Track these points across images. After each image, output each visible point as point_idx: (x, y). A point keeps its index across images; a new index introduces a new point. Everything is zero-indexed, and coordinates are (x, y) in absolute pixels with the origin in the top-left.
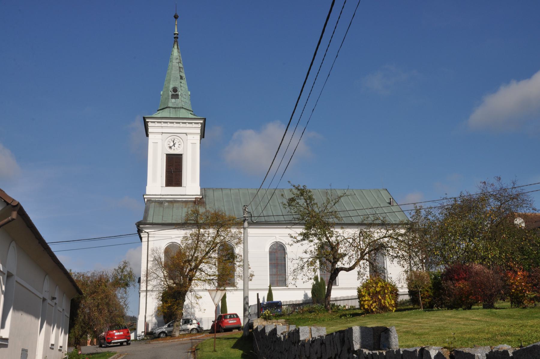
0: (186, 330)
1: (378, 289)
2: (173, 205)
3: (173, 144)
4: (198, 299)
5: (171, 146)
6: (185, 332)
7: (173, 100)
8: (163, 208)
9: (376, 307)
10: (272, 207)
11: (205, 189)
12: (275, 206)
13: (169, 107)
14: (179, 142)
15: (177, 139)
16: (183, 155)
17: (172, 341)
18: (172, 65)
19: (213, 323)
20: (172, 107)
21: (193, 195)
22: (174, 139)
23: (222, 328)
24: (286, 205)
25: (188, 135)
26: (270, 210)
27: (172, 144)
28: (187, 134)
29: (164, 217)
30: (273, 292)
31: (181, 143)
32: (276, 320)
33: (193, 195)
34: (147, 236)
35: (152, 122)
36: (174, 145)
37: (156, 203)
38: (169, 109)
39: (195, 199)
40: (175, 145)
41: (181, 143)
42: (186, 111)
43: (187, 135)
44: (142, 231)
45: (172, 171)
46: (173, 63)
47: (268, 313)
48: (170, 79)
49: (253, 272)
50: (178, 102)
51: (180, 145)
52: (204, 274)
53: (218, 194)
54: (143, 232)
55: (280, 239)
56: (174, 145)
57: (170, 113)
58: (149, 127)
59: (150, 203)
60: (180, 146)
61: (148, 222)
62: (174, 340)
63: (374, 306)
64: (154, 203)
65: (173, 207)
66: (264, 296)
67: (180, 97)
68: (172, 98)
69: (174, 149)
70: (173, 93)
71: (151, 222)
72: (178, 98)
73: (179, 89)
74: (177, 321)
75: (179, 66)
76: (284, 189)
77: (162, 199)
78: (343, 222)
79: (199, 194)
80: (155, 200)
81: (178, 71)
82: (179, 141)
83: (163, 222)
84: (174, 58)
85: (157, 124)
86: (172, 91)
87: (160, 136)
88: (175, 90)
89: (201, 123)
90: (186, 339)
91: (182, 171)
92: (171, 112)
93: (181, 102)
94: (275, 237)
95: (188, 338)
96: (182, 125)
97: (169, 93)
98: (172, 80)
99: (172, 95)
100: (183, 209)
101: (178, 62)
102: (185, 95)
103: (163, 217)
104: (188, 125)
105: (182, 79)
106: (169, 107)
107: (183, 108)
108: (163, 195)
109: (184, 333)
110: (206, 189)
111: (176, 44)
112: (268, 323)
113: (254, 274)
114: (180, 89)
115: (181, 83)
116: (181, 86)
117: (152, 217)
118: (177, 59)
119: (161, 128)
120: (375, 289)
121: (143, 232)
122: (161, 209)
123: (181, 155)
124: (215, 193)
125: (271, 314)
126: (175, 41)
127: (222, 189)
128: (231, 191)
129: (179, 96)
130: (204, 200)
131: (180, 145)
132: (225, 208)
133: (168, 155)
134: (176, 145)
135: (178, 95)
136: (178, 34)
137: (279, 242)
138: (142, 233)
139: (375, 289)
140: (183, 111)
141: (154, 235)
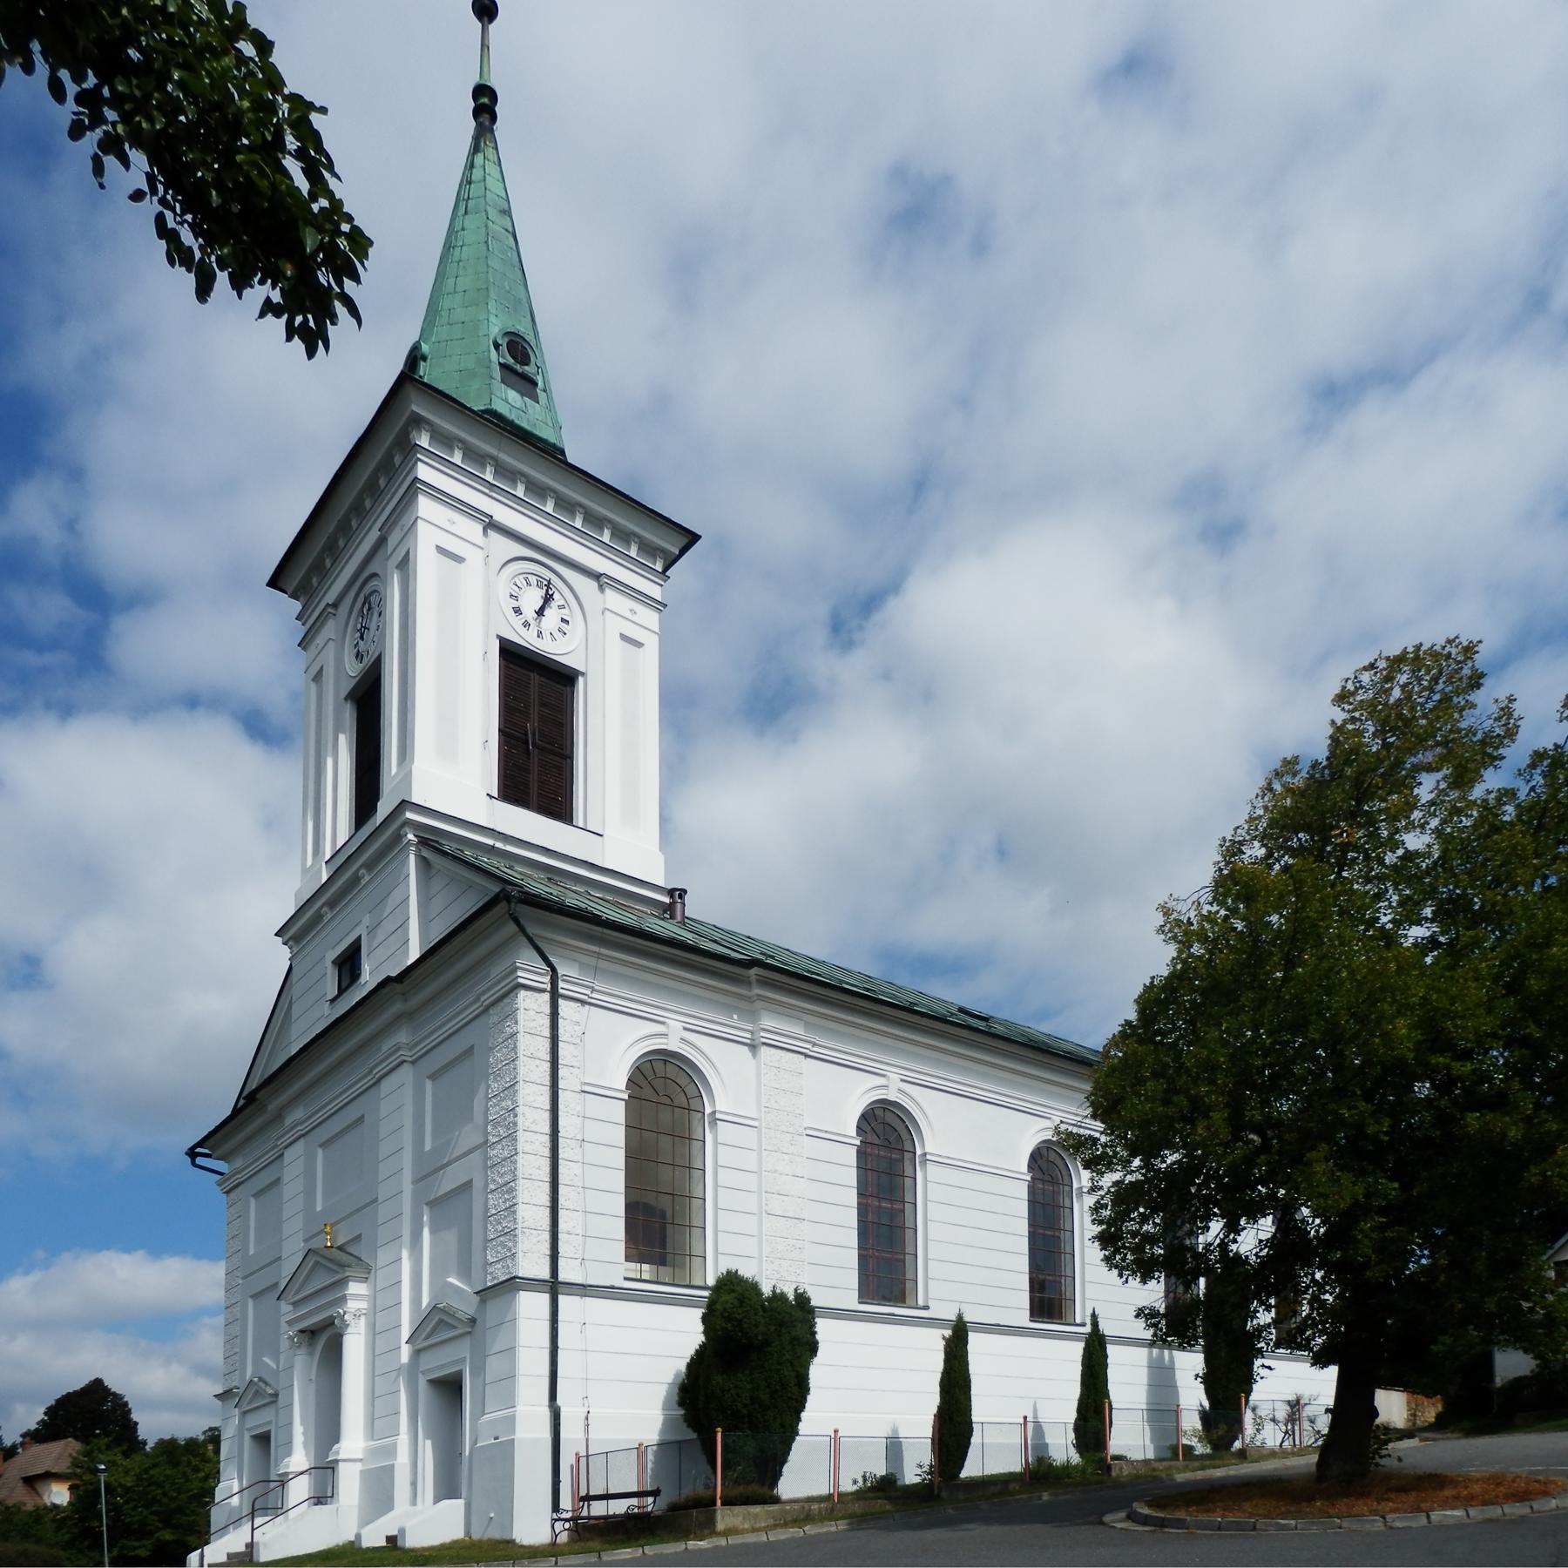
7: (513, 395)
16: (581, 679)
31: (572, 617)
35: (438, 436)
43: (601, 588)
70: (511, 361)
87: (474, 529)
98: (492, 295)
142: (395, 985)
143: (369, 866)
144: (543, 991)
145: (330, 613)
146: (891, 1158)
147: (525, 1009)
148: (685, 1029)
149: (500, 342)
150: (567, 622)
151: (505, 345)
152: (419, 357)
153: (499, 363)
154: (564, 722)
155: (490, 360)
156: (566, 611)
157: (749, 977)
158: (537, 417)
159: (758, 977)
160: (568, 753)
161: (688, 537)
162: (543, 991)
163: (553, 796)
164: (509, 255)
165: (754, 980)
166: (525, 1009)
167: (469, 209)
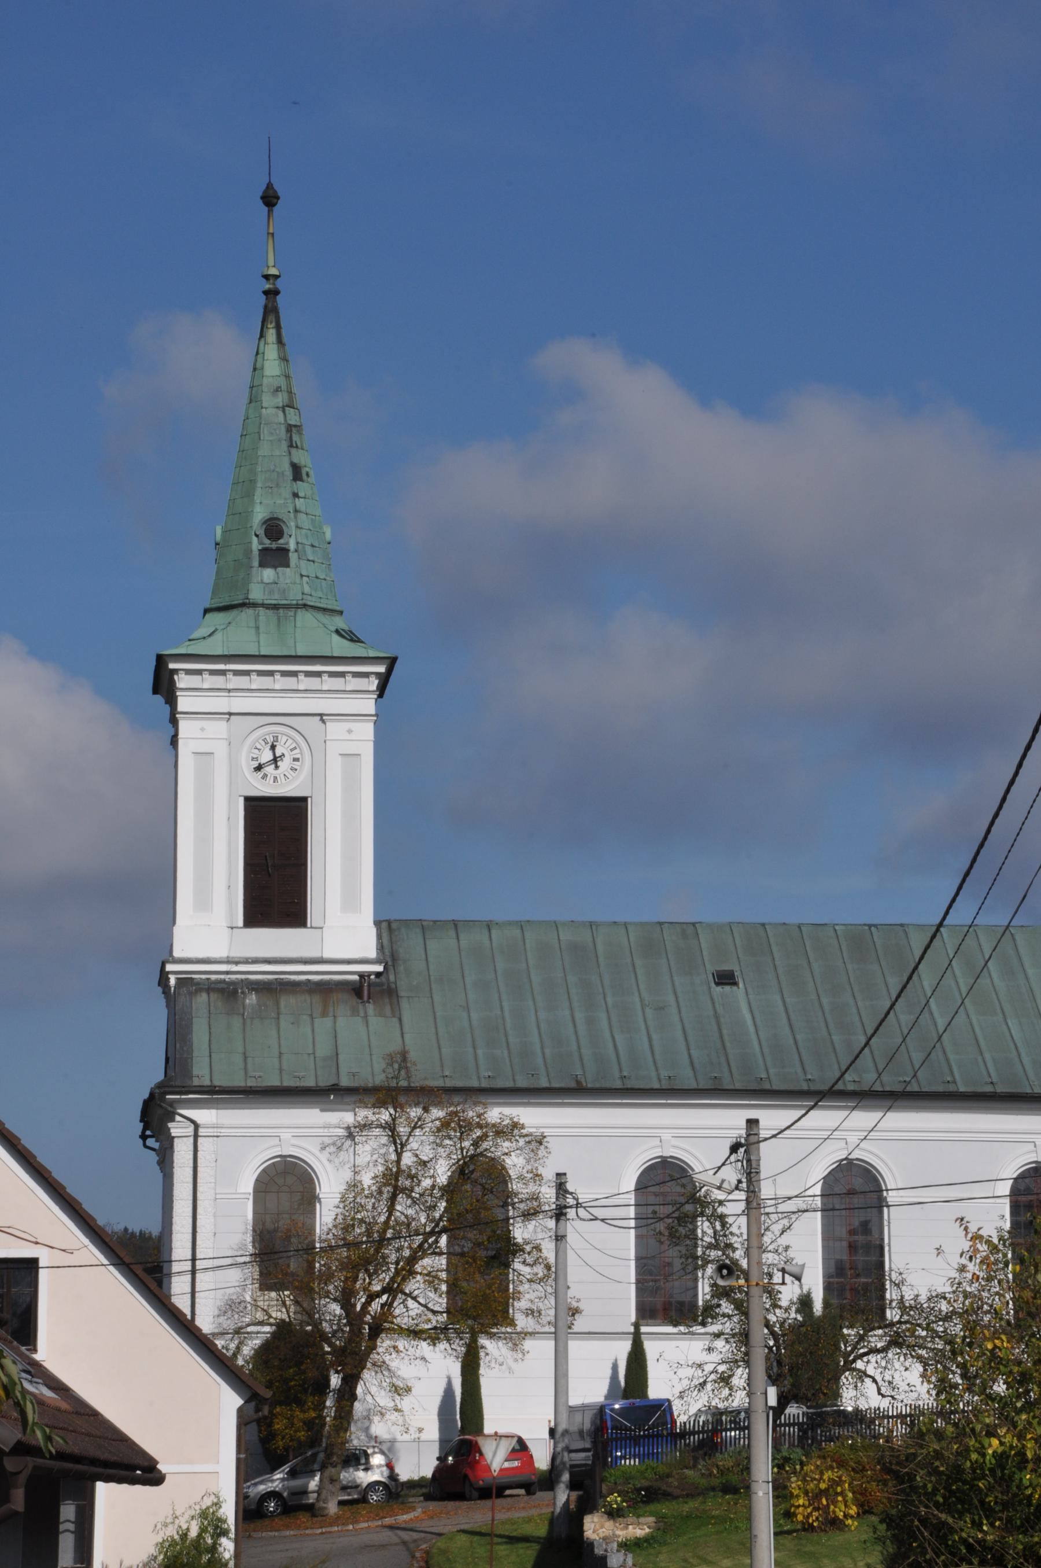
0: (351, 1487)
1: (823, 1486)
2: (278, 1004)
3: (271, 757)
4: (399, 1395)
5: (263, 761)
6: (349, 1495)
7: (268, 574)
8: (241, 1020)
9: (820, 1519)
10: (648, 1011)
11: (389, 922)
12: (660, 1009)
13: (254, 605)
14: (295, 748)
15: (284, 738)
16: (309, 800)
17: (322, 1533)
18: (260, 416)
19: (437, 1462)
20: (263, 605)
21: (349, 962)
22: (276, 739)
23: (471, 1485)
24: (664, 1235)
25: (327, 724)
26: (643, 1027)
27: (267, 756)
28: (324, 718)
29: (249, 1060)
30: (651, 1348)
31: (301, 753)
32: (635, 1518)
33: (349, 962)
34: (192, 1133)
36: (275, 760)
37: (212, 995)
38: (250, 611)
39: (356, 977)
40: (279, 763)
41: (301, 753)
42: (320, 616)
43: (323, 721)
44: (174, 1113)
45: (270, 864)
46: (264, 410)
47: (616, 1501)
48: (253, 482)
49: (578, 1301)
50: (288, 581)
51: (296, 760)
52: (416, 1305)
53: (441, 947)
54: (178, 1118)
55: (674, 1147)
56: (275, 760)
57: (257, 628)
58: (178, 694)
59: (191, 994)
60: (296, 765)
61: (196, 1082)
62: (328, 1529)
63: (814, 1518)
64: (204, 996)
65: (278, 1014)
66: (616, 1360)
67: (293, 557)
68: (262, 565)
69: (275, 778)
71: (207, 1083)
72: (288, 566)
73: (290, 527)
74: (331, 1464)
75: (285, 420)
76: (697, 925)
77: (234, 977)
78: (916, 1089)
79: (373, 954)
80: (208, 979)
81: (284, 445)
82: (294, 745)
83: (249, 1084)
84: (265, 389)
85: (209, 681)
88: (274, 529)
89: (378, 675)
90: (365, 1525)
92: (261, 630)
93: (298, 581)
94: (657, 1142)
95: (370, 1523)
96: (305, 683)
97: (251, 543)
98: (259, 484)
99: (264, 552)
100: (316, 1020)
101: (281, 405)
102: (313, 546)
103: (245, 1058)
104: (329, 683)
105: (301, 480)
106: (254, 605)
107: (305, 606)
108: (237, 963)
109: (346, 1498)
110: (394, 926)
111: (273, 325)
112: (617, 1525)
113: (582, 1305)
114: (293, 524)
115: (296, 495)
116: (296, 511)
117: (207, 1059)
118: (278, 389)
119: (227, 694)
120: (817, 1486)
121: (178, 1118)
122: (236, 1022)
123: (304, 800)
124: (432, 945)
125: (624, 1504)
126: (266, 307)
127: (456, 926)
128: (493, 932)
129: (290, 554)
130: (392, 978)
131: (296, 760)
132: (474, 1016)
133: (251, 802)
134: (284, 765)
135: (287, 551)
136: (276, 277)
137: (671, 1157)
138: (173, 1120)
139: (817, 1486)
140: (306, 618)
141: (219, 1130)
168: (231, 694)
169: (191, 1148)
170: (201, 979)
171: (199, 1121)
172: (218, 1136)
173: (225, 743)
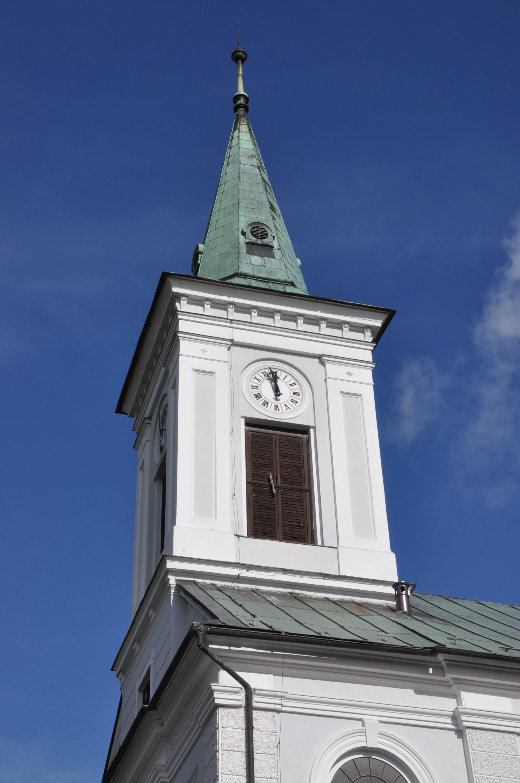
7: (256, 259)
14: (294, 384)
16: (312, 431)
25: (328, 365)
31: (301, 389)
34: (243, 703)
35: (193, 301)
41: (301, 389)
43: (322, 363)
58: (179, 317)
60: (296, 398)
67: (277, 253)
70: (253, 239)
82: (293, 381)
86: (248, 231)
87: (221, 352)
91: (310, 490)
98: (242, 205)
108: (249, 567)
111: (245, 123)
119: (228, 324)
123: (305, 430)
142: (150, 712)
143: (153, 607)
144: (239, 707)
145: (147, 423)
146: (284, 644)
147: (223, 728)
148: (381, 722)
149: (245, 231)
150: (298, 394)
151: (249, 232)
152: (198, 253)
153: (246, 243)
154: (302, 465)
155: (239, 243)
156: (296, 387)
157: (440, 663)
158: (273, 266)
159: (447, 662)
160: (307, 487)
161: (387, 313)
162: (239, 707)
163: (296, 524)
164: (255, 179)
165: (445, 666)
166: (223, 728)
167: (229, 162)
168: (234, 325)
169: (242, 724)
170: (205, 584)
171: (252, 686)
172: (278, 711)
173: (226, 366)
